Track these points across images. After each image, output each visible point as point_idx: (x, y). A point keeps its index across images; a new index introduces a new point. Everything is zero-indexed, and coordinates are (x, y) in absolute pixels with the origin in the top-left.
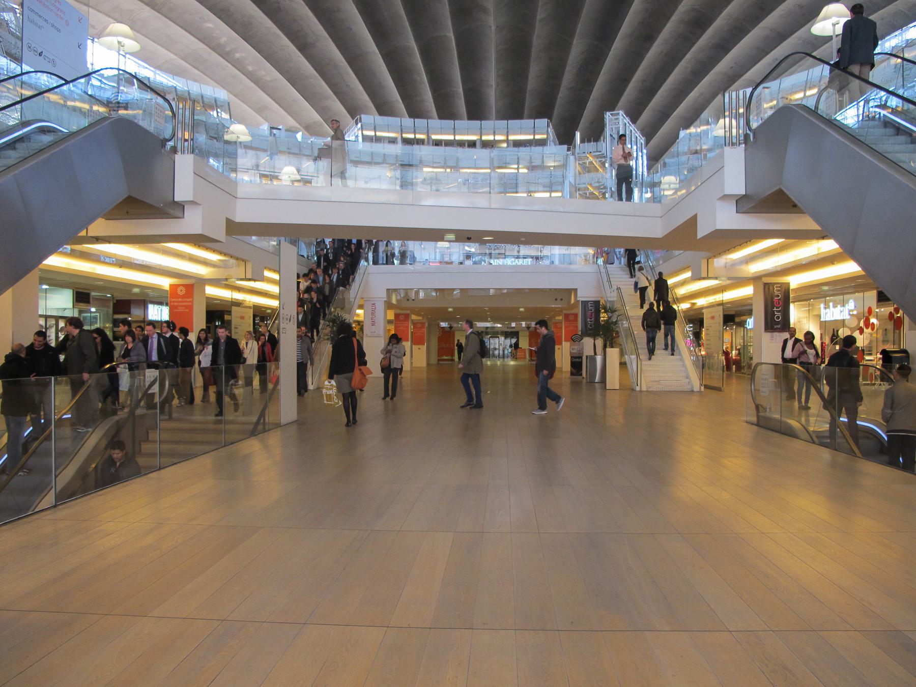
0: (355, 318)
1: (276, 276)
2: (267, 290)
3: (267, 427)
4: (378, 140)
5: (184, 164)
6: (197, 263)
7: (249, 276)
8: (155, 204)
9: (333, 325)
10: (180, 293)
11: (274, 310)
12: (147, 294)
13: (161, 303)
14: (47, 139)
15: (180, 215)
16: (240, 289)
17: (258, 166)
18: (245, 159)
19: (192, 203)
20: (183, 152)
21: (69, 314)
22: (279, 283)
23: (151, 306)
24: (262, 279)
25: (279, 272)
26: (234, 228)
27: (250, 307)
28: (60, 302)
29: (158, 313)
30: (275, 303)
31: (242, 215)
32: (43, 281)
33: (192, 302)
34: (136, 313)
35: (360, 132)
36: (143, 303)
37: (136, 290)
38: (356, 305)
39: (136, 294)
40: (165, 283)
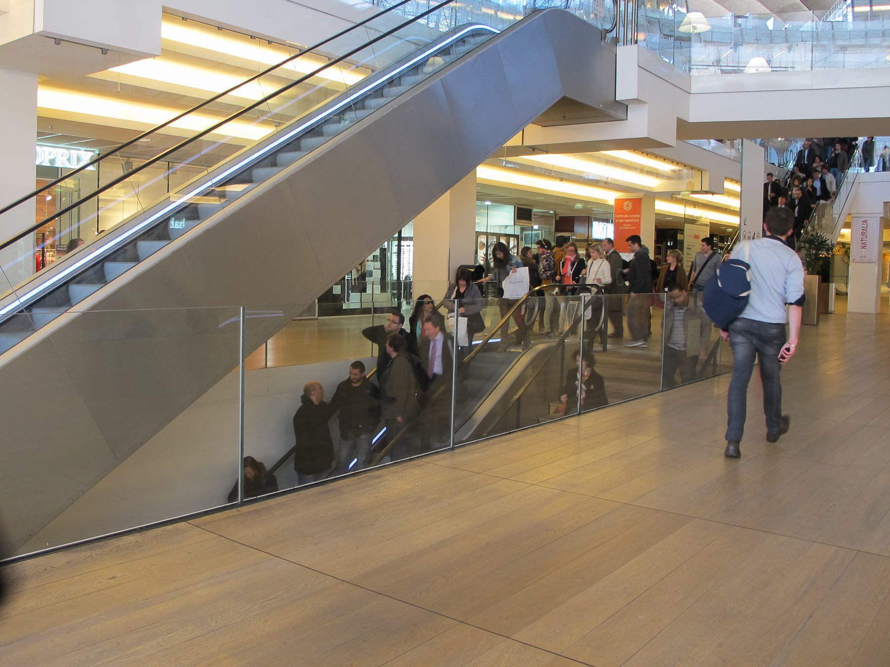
0: (839, 240)
1: (736, 188)
2: (728, 204)
3: (718, 370)
4: (874, 16)
5: (627, 57)
6: (644, 173)
7: (705, 188)
8: (594, 105)
9: (810, 248)
10: (625, 208)
11: (736, 229)
12: (591, 210)
13: (606, 221)
14: (479, 39)
15: (624, 117)
16: (696, 204)
17: (718, 61)
18: (700, 53)
19: (637, 101)
20: (625, 43)
21: (510, 231)
22: (740, 196)
23: (595, 224)
24: (722, 191)
25: (739, 181)
26: (687, 130)
27: (706, 225)
28: (501, 219)
29: (602, 231)
30: (734, 220)
31: (696, 114)
32: (481, 197)
33: (639, 219)
34: (580, 230)
35: (850, 9)
36: (588, 220)
37: (579, 206)
38: (841, 222)
39: (578, 210)
40: (610, 197)
